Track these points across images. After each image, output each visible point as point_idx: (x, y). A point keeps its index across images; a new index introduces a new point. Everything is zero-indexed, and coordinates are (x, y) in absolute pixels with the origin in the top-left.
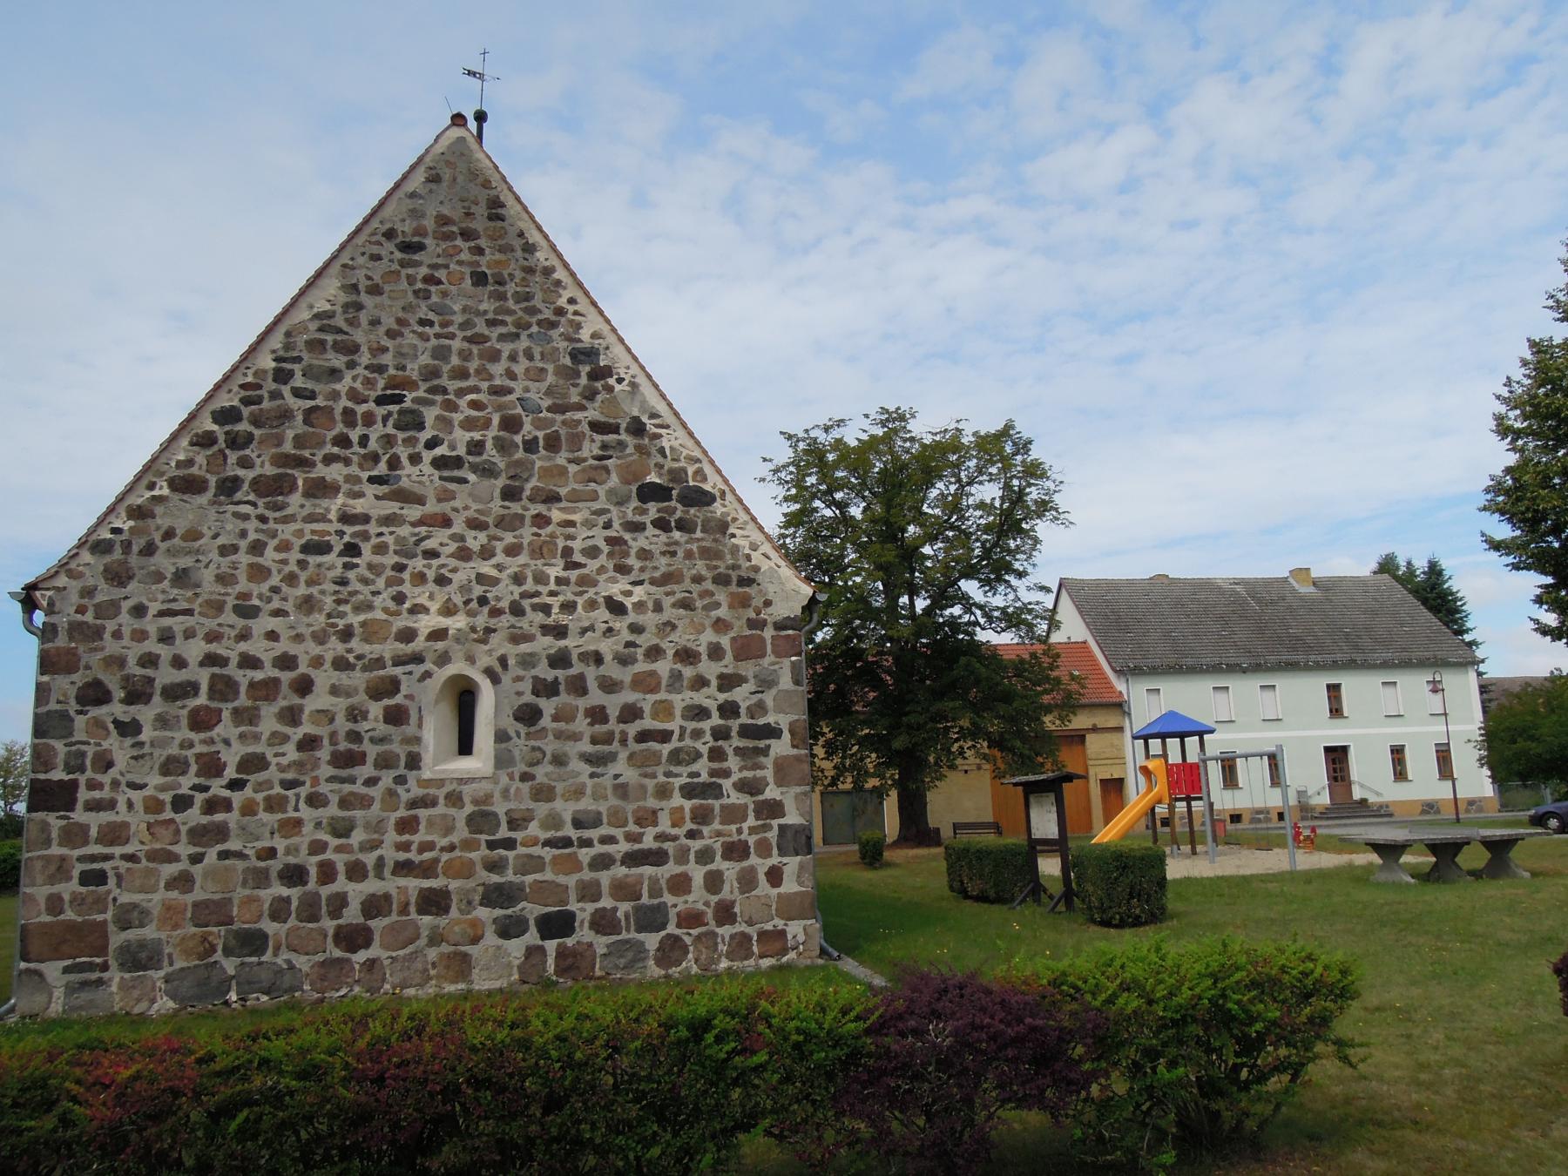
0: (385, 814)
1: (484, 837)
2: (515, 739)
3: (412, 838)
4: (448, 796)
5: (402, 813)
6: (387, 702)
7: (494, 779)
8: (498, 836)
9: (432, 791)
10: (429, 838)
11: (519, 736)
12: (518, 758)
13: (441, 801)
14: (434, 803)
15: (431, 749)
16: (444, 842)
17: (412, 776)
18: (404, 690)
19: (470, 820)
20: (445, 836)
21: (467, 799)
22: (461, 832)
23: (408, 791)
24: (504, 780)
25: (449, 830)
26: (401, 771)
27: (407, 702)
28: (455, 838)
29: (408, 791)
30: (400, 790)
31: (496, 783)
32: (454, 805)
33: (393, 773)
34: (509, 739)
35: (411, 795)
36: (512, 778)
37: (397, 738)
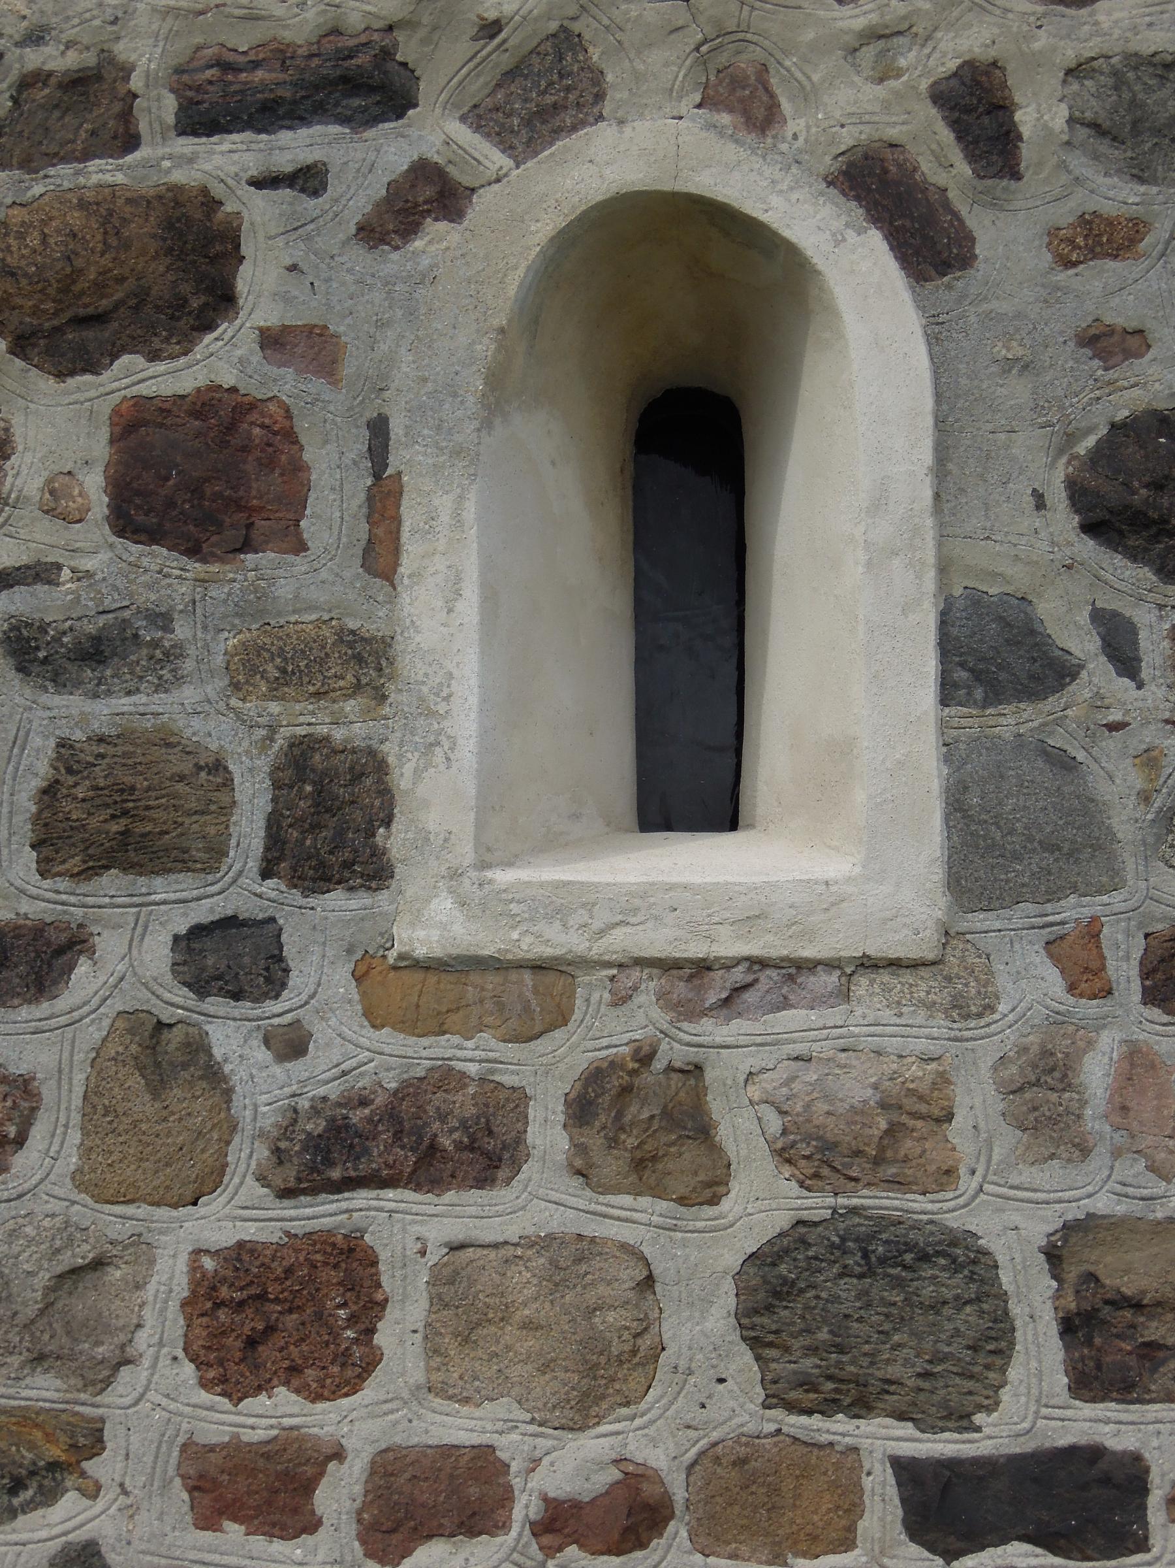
0: (114, 1222)
1: (882, 1439)
2: (1098, 673)
3: (324, 1419)
4: (598, 1100)
5: (242, 1214)
6: (138, 376)
7: (942, 974)
8: (996, 1435)
9: (472, 1053)
10: (455, 1426)
11: (1122, 653)
12: (1126, 821)
13: (547, 1133)
14: (483, 1151)
15: (465, 722)
16: (573, 1465)
17: (319, 933)
18: (263, 289)
19: (773, 1290)
20: (581, 1411)
21: (742, 1131)
22: (704, 1395)
23: (291, 1044)
24: (1030, 984)
25: (606, 1371)
26: (241, 887)
27: (284, 383)
28: (654, 1436)
29: (291, 1044)
30: (232, 1035)
31: (970, 1007)
32: (644, 1172)
33: (180, 903)
34: (1052, 673)
35: (319, 1076)
36: (1085, 974)
37: (208, 645)
